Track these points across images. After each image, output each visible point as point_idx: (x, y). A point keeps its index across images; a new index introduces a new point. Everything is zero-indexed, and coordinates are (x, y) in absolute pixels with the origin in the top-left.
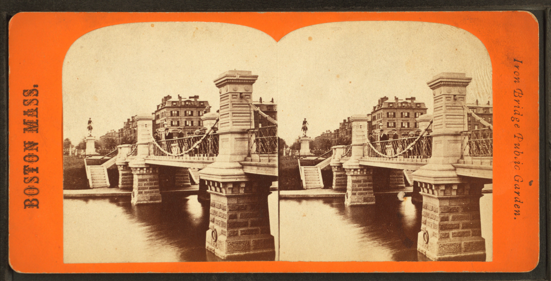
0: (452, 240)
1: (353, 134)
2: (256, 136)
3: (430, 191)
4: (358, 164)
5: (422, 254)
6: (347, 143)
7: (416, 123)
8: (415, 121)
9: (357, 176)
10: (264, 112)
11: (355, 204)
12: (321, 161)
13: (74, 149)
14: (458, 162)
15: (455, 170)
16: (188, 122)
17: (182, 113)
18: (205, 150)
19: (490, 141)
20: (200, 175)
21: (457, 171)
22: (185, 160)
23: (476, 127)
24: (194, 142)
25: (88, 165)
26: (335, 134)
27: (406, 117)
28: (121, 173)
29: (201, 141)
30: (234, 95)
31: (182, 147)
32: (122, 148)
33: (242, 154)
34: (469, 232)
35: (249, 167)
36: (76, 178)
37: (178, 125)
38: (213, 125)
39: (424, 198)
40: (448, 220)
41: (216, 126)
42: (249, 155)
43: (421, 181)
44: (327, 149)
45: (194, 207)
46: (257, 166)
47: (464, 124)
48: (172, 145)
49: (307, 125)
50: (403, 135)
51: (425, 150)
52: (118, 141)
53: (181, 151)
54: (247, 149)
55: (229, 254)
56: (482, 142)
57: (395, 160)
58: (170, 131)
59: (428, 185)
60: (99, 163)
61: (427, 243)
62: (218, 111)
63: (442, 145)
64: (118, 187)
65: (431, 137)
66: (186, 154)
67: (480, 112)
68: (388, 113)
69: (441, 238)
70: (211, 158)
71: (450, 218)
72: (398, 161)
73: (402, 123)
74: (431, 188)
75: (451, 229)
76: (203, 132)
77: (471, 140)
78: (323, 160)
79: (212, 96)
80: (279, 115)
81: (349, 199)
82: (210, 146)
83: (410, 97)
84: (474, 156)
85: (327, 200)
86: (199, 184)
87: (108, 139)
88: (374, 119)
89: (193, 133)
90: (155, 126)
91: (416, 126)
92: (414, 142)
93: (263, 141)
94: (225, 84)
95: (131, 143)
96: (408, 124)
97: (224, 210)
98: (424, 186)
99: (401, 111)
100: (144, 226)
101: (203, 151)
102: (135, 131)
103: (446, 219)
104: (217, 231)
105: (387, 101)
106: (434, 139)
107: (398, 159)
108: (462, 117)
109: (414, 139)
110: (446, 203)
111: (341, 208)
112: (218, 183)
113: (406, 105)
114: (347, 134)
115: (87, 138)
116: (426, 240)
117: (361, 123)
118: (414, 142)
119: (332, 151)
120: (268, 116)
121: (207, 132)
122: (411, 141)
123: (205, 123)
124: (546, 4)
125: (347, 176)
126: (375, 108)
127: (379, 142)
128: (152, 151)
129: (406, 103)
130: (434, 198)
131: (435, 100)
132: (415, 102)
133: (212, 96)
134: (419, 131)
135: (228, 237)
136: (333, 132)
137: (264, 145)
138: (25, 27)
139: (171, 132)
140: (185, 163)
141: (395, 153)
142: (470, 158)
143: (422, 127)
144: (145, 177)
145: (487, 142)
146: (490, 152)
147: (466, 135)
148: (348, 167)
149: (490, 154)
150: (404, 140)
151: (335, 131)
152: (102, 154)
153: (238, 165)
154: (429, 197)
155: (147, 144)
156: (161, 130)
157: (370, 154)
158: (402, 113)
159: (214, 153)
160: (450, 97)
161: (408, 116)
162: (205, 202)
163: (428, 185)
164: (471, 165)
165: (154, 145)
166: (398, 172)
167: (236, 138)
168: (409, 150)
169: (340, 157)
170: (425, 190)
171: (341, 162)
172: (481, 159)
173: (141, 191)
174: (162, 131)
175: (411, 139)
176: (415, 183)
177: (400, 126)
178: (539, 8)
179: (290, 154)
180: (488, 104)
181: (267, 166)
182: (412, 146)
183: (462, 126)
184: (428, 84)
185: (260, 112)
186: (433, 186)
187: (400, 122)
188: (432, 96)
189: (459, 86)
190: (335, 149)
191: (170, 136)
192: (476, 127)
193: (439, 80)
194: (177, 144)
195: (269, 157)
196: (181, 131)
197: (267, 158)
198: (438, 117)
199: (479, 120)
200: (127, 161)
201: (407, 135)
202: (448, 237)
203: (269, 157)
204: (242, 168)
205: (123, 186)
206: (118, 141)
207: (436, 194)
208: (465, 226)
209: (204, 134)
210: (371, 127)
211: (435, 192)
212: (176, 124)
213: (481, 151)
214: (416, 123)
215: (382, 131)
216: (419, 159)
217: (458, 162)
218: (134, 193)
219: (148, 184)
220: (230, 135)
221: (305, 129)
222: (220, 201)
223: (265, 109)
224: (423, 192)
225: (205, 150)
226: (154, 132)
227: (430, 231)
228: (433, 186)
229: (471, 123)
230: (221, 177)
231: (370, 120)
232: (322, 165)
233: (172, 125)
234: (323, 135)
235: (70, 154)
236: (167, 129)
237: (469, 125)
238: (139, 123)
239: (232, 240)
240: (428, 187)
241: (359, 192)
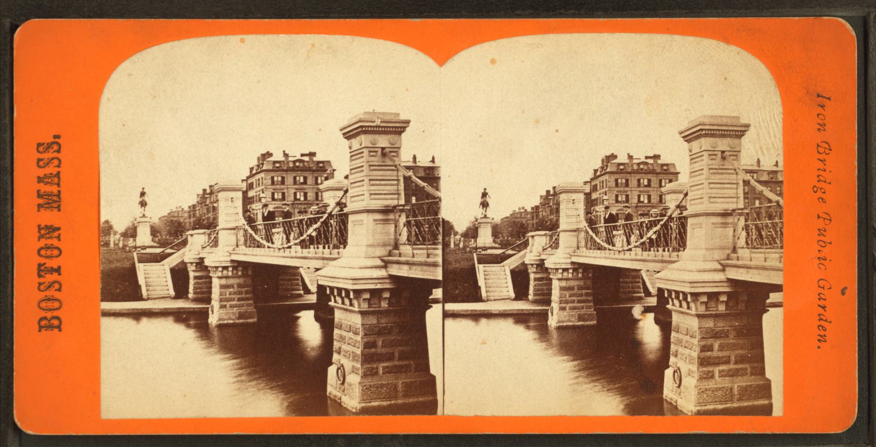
0: (719, 382)
1: (561, 214)
2: (407, 217)
3: (347, 301)
5: (671, 403)
6: (551, 227)
7: (661, 196)
8: (659, 193)
9: (567, 279)
10: (420, 178)
11: (565, 324)
12: (510, 256)
13: (118, 236)
14: (728, 258)
15: (723, 270)
16: (298, 194)
17: (289, 180)
19: (780, 225)
20: (319, 278)
22: (293, 254)
23: (757, 202)
24: (308, 226)
25: (140, 262)
26: (532, 213)
27: (646, 186)
28: (192, 275)
29: (319, 224)
30: (372, 150)
31: (290, 234)
32: (195, 236)
33: (384, 245)
34: (746, 369)
35: (396, 266)
36: (122, 284)
37: (283, 198)
38: (338, 200)
39: (674, 315)
40: (712, 350)
41: (343, 201)
42: (396, 246)
44: (519, 237)
45: (309, 329)
46: (409, 264)
49: (488, 199)
50: (641, 215)
51: (676, 238)
52: (188, 225)
53: (288, 241)
54: (392, 237)
55: (364, 405)
56: (767, 226)
57: (627, 255)
58: (271, 208)
59: (681, 295)
60: (158, 259)
61: (343, 383)
62: (346, 177)
63: (703, 232)
65: (346, 215)
67: (762, 179)
68: (616, 180)
69: (701, 379)
70: (336, 251)
71: (716, 346)
73: (639, 196)
74: (685, 299)
76: (323, 209)
77: (749, 222)
78: (513, 255)
79: (337, 153)
80: (443, 183)
81: (555, 317)
82: (334, 233)
83: (307, 152)
84: (754, 248)
86: (317, 292)
87: (172, 221)
88: (595, 189)
89: (306, 212)
90: (247, 201)
91: (661, 201)
92: (659, 227)
93: (418, 225)
94: (358, 134)
95: (208, 228)
96: (649, 197)
97: (356, 333)
98: (673, 296)
99: (638, 176)
100: (229, 359)
101: (323, 240)
102: (215, 209)
103: (710, 348)
104: (345, 367)
105: (615, 161)
107: (293, 250)
108: (735, 186)
109: (659, 221)
110: (710, 324)
111: (543, 331)
112: (347, 292)
113: (646, 167)
114: (551, 213)
115: (139, 220)
116: (678, 382)
117: (574, 196)
118: (659, 227)
119: (528, 240)
120: (764, 188)
121: (329, 210)
122: (654, 224)
123: (326, 195)
124: (868, 7)
125: (551, 279)
126: (596, 171)
127: (603, 226)
128: (242, 240)
129: (646, 164)
130: (691, 315)
131: (692, 159)
132: (659, 162)
133: (337, 153)
134: (666, 209)
135: (362, 377)
136: (529, 210)
137: (420, 230)
138: (39, 43)
139: (271, 210)
140: (295, 260)
141: (629, 243)
142: (409, 247)
143: (671, 201)
144: (231, 281)
145: (774, 225)
146: (778, 242)
147: (741, 214)
148: (553, 266)
149: (779, 244)
150: (642, 223)
151: (533, 208)
153: (379, 262)
154: (682, 313)
155: (234, 229)
156: (257, 207)
157: (589, 246)
158: (639, 180)
159: (340, 243)
160: (716, 155)
161: (649, 185)
162: (326, 322)
163: (681, 295)
164: (748, 263)
165: (245, 231)
166: (634, 273)
167: (375, 220)
168: (650, 238)
169: (540, 249)
170: (676, 302)
171: (543, 257)
172: (764, 253)
174: (257, 208)
175: (654, 221)
176: (660, 291)
177: (635, 200)
178: (857, 12)
179: (461, 245)
180: (777, 165)
181: (424, 264)
183: (735, 200)
184: (680, 134)
185: (414, 178)
186: (689, 296)
187: (636, 193)
188: (687, 153)
189: (730, 136)
191: (270, 216)
192: (757, 202)
193: (698, 128)
194: (281, 229)
195: (428, 249)
196: (287, 209)
197: (425, 251)
198: (696, 186)
199: (762, 191)
200: (201, 256)
202: (712, 377)
203: (428, 249)
204: (385, 267)
205: (195, 296)
206: (188, 225)
208: (740, 360)
209: (324, 213)
210: (590, 203)
211: (692, 305)
212: (280, 197)
213: (765, 240)
214: (661, 196)
215: (607, 208)
216: (666, 253)
217: (728, 258)
218: (212, 307)
219: (235, 293)
220: (365, 215)
221: (485, 205)
222: (349, 319)
223: (422, 174)
224: (673, 305)
225: (326, 238)
226: (245, 211)
228: (689, 296)
229: (749, 196)
230: (351, 282)
231: (588, 190)
232: (512, 263)
233: (273, 199)
234: (513, 215)
235: (112, 245)
236: (265, 206)
237: (745, 198)
238: (221, 195)
239: (369, 381)
240: (681, 298)
241: (570, 305)
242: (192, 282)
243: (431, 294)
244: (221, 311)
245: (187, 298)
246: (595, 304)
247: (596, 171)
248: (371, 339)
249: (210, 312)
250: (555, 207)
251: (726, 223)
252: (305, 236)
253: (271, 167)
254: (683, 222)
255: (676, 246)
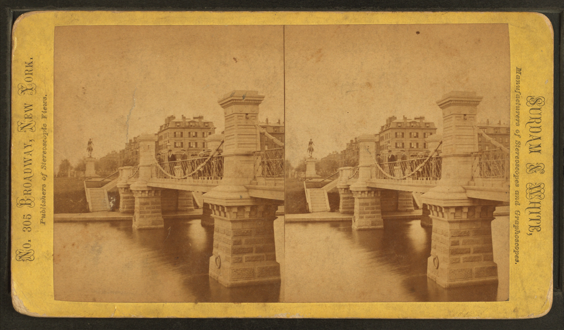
3: (222, 214)
4: (146, 186)
5: (432, 280)
6: (355, 164)
8: (203, 141)
13: (293, 171)
15: (465, 192)
17: (421, 134)
18: (428, 173)
19: (502, 163)
21: (250, 193)
28: (341, 196)
38: (217, 147)
39: (434, 221)
40: (241, 244)
41: (439, 149)
43: (213, 203)
44: (333, 171)
45: (416, 232)
46: (264, 190)
47: (256, 144)
48: (175, 167)
49: (314, 147)
50: (412, 156)
51: (435, 171)
52: (340, 163)
53: (185, 174)
56: (493, 163)
57: (403, 182)
59: (438, 208)
61: (219, 268)
62: (223, 133)
64: (338, 211)
66: (190, 176)
67: (490, 133)
68: (396, 133)
69: (234, 263)
70: (216, 180)
71: (461, 242)
72: (407, 184)
73: (411, 144)
74: (223, 210)
75: (245, 253)
77: (482, 161)
79: (216, 117)
80: (288, 136)
82: (214, 169)
83: (198, 116)
84: (485, 177)
85: (334, 224)
87: (330, 161)
89: (196, 155)
92: (423, 164)
94: (449, 105)
95: (132, 165)
96: (196, 144)
98: (433, 209)
99: (189, 130)
103: (239, 243)
106: (444, 160)
107: (187, 180)
109: (424, 160)
111: (349, 231)
115: (87, 160)
116: (219, 265)
117: (149, 143)
118: (423, 164)
121: (211, 154)
122: (420, 161)
123: (429, 145)
126: (383, 127)
128: (155, 172)
130: (227, 221)
131: (226, 119)
132: (203, 121)
133: (216, 117)
134: (428, 152)
135: (232, 264)
136: (118, 152)
137: (270, 168)
139: (174, 154)
141: (404, 174)
142: (480, 179)
143: (432, 147)
148: (355, 190)
149: (501, 175)
150: (412, 161)
152: (324, 176)
153: (461, 189)
154: (221, 219)
155: (149, 166)
157: (378, 175)
158: (189, 133)
160: (460, 117)
161: (196, 136)
162: (210, 229)
164: (481, 187)
165: (157, 167)
166: (408, 194)
168: (418, 172)
170: (217, 212)
171: (129, 183)
173: (362, 215)
175: (421, 160)
176: (425, 206)
177: (187, 146)
179: (75, 176)
180: (279, 123)
181: (268, 188)
182: (421, 167)
184: (219, 102)
186: (226, 209)
189: (251, 104)
190: (342, 170)
191: (173, 158)
192: (487, 147)
194: (180, 166)
195: (275, 180)
196: (184, 153)
197: (273, 181)
200: (348, 184)
201: (416, 156)
202: (459, 262)
203: (275, 180)
204: (248, 191)
205: (344, 210)
206: (340, 163)
207: (229, 217)
208: (477, 251)
211: (228, 214)
212: (401, 146)
215: (390, 151)
217: (468, 184)
219: (149, 208)
223: (272, 131)
224: (215, 214)
227: (441, 256)
228: (226, 209)
230: (443, 202)
233: (175, 147)
235: (69, 176)
236: (170, 151)
237: (479, 145)
240: (220, 210)
242: (341, 201)
243: (494, 210)
244: (142, 219)
245: (338, 211)
246: (382, 215)
247: (161, 127)
248: (238, 239)
249: (353, 221)
250: (356, 151)
251: (249, 161)
252: (195, 171)
253: (174, 126)
254: (439, 160)
255: (435, 176)
